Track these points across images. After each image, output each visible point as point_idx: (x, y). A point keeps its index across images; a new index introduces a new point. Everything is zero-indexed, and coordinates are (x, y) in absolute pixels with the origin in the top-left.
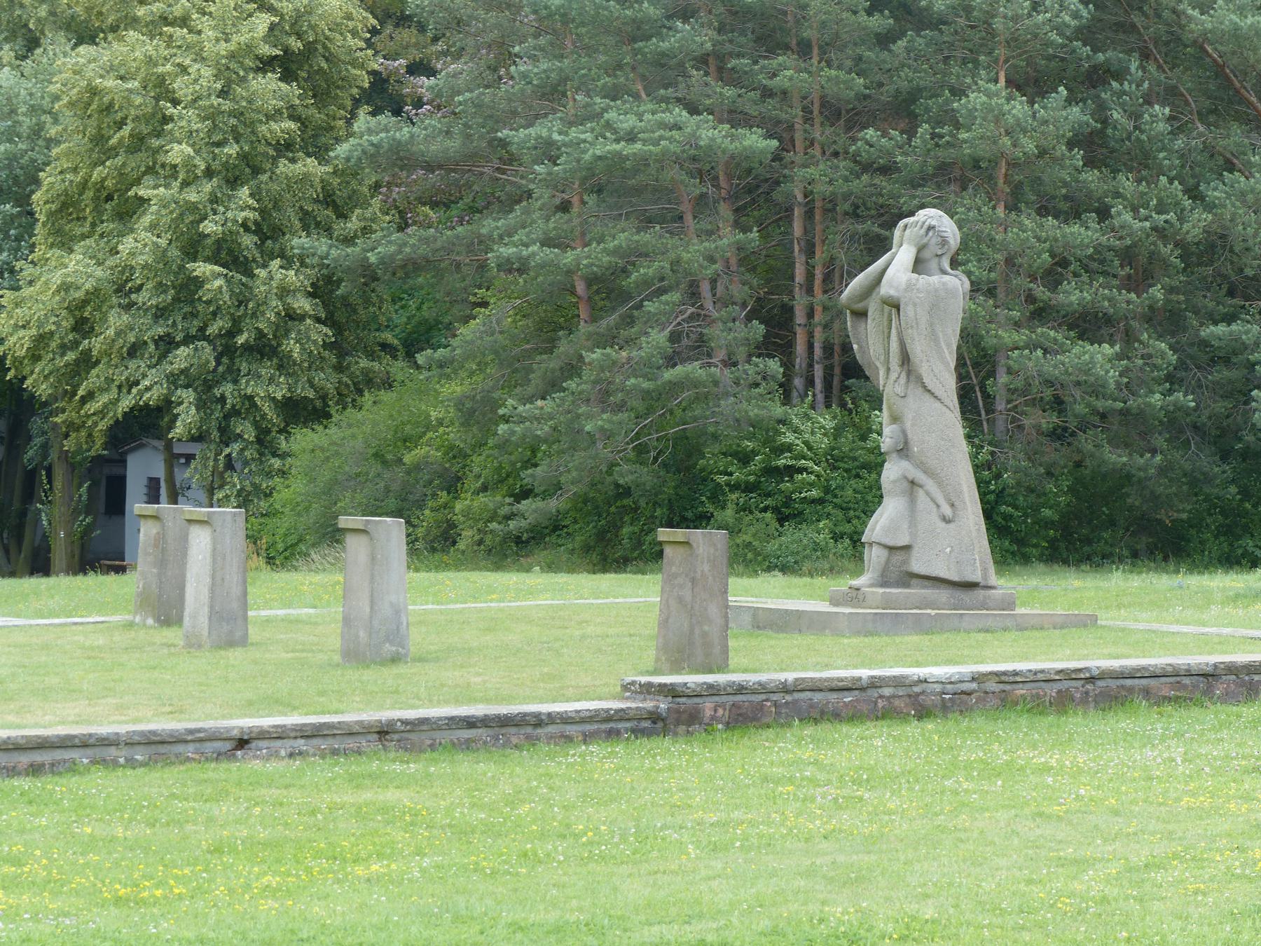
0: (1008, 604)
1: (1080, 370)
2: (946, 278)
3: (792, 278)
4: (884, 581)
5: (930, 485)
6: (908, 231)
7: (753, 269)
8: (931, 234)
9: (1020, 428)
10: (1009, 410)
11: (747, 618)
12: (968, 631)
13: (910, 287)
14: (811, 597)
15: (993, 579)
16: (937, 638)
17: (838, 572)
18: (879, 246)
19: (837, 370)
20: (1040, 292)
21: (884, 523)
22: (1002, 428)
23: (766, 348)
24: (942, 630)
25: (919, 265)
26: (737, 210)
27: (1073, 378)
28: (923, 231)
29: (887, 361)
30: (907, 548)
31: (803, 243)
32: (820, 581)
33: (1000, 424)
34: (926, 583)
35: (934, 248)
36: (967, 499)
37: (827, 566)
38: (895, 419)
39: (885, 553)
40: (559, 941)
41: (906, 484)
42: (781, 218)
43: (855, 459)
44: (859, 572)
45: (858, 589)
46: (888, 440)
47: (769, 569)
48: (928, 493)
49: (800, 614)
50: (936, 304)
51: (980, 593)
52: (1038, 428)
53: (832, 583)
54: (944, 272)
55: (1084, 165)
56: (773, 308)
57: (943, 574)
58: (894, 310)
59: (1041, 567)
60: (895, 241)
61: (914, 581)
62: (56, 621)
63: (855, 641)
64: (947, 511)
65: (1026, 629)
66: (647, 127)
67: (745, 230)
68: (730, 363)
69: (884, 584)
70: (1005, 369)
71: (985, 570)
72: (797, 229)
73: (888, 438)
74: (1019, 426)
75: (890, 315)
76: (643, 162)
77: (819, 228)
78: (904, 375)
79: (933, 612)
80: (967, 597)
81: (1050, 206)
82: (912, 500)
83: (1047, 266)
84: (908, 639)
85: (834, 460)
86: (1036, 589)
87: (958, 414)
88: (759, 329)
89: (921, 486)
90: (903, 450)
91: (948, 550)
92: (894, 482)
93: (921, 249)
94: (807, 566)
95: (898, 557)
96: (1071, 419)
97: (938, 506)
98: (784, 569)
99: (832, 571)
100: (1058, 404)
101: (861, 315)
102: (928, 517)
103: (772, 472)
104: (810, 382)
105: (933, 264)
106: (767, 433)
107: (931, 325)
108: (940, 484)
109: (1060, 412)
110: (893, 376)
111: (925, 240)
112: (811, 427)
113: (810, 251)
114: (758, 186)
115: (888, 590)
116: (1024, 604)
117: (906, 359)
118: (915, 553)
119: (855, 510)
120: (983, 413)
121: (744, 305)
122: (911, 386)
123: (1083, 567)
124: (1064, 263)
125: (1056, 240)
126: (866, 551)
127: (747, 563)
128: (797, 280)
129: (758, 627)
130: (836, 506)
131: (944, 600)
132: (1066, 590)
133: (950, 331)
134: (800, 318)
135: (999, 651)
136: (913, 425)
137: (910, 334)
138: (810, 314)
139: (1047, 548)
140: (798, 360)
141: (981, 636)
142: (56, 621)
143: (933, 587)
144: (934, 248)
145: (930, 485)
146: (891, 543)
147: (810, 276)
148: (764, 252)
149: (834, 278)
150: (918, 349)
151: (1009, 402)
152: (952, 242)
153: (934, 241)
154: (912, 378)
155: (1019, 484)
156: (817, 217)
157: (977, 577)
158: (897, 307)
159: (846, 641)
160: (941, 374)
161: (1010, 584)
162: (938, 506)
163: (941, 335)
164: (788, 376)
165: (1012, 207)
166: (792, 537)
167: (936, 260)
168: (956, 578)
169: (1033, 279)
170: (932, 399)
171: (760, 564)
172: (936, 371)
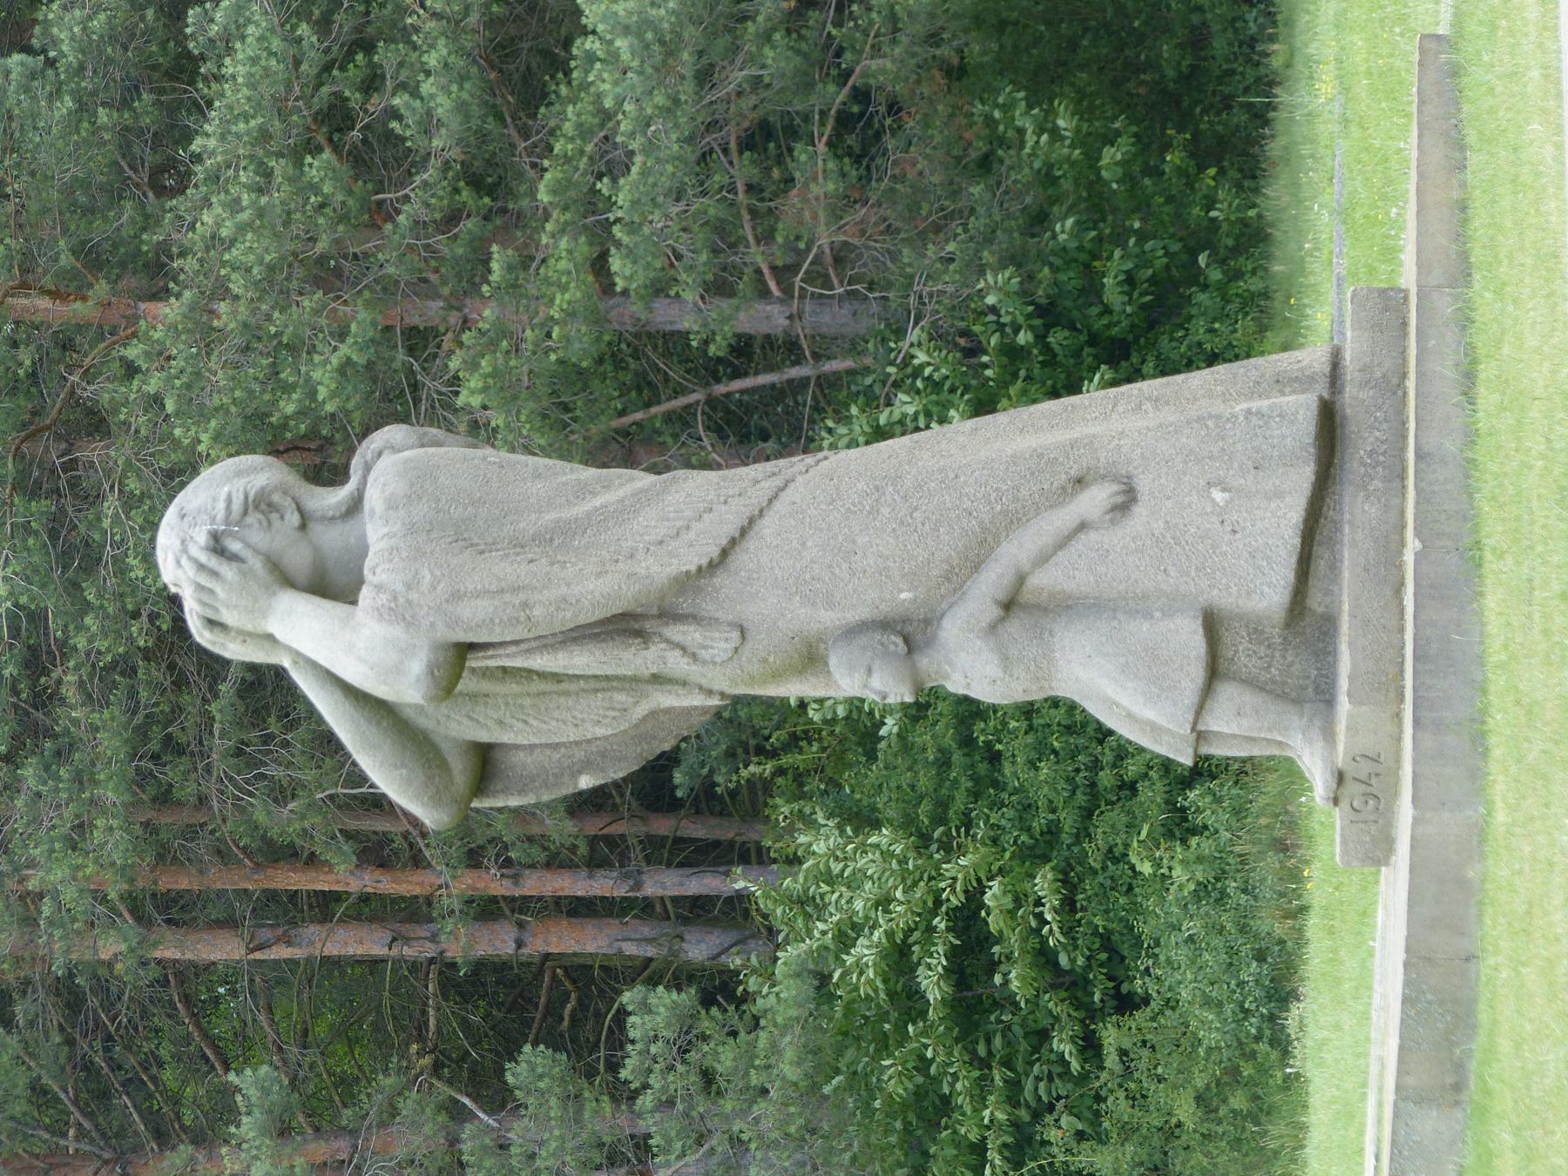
0: (1386, 309)
1: (663, 69)
2: (374, 498)
3: (375, 963)
4: (1317, 696)
5: (1015, 551)
6: (228, 617)
7: (347, 1086)
8: (234, 546)
9: (841, 256)
10: (787, 291)
11: (1429, 1123)
12: (1470, 437)
13: (399, 612)
14: (1366, 914)
15: (1312, 356)
16: (1493, 533)
17: (1292, 825)
18: (268, 691)
19: (662, 826)
20: (419, 199)
21: (1138, 698)
22: (845, 311)
23: (592, 1041)
24: (1468, 516)
25: (333, 584)
26: (162, 1137)
27: (687, 91)
28: (228, 571)
29: (632, 683)
30: (1212, 624)
31: (265, 934)
32: (1318, 887)
33: (833, 318)
34: (1320, 566)
35: (281, 536)
36: (1062, 436)
37: (1272, 860)
38: (811, 658)
39: (1228, 693)
41: (1014, 627)
42: (187, 999)
43: (944, 763)
44: (1292, 774)
45: (1341, 778)
46: (876, 682)
47: (1282, 1045)
48: (1043, 559)
49: (1417, 959)
50: (455, 530)
51: (1353, 397)
52: (841, 205)
53: (1321, 847)
54: (355, 506)
55: (28, 50)
56: (465, 1024)
57: (1293, 512)
58: (474, 662)
59: (1275, 193)
60: (258, 656)
61: (1316, 602)
62: (1412, 425)
63: (1500, 787)
64: (1096, 499)
65: (1464, 256)
67: (224, 1109)
69: (1324, 696)
70: (660, 304)
71: (1282, 382)
72: (223, 949)
73: (863, 680)
74: (838, 261)
75: (486, 673)
77: (221, 880)
78: (675, 632)
79: (1412, 545)
80: (1363, 439)
81: (150, 158)
82: (1063, 607)
83: (345, 170)
84: (1494, 625)
85: (932, 833)
86: (1343, 214)
87: (794, 465)
88: (533, 1068)
89: (1021, 579)
90: (909, 634)
91: (1218, 496)
92: (1006, 662)
93: (285, 579)
94: (1269, 924)
95: (1241, 652)
96: (815, 101)
97: (1082, 527)
98: (1281, 993)
99: (1287, 843)
100: (768, 138)
101: (486, 762)
102: (1108, 558)
104: (697, 910)
105: (331, 538)
106: (856, 1029)
107: (519, 545)
108: (1013, 521)
109: (792, 133)
110: (677, 664)
111: (256, 563)
112: (846, 886)
114: (88, 1066)
115: (1343, 684)
116: (1390, 253)
117: (626, 626)
118: (1226, 598)
119: (1096, 765)
120: (795, 372)
121: (457, 1114)
122: (708, 608)
123: (1276, 62)
124: (336, 118)
125: (264, 136)
126: (1218, 750)
127: (1260, 1111)
128: (378, 950)
129: (1458, 1087)
130: (1083, 834)
131: (1373, 510)
132: (1345, 122)
133: (538, 488)
134: (498, 942)
135: (1532, 342)
136: (830, 604)
137: (546, 613)
138: (486, 910)
139: (1222, 172)
140: (630, 949)
141: (1486, 397)
142: (1412, 425)
143: (1333, 543)
144: (281, 536)
146: (1195, 673)
147: (369, 909)
148: (293, 1051)
149: (383, 841)
150: (594, 587)
151: (764, 293)
152: (260, 480)
153: (257, 537)
154: (685, 606)
155: (1014, 259)
156: (183, 883)
157: (1302, 408)
158: (465, 649)
159: (1501, 817)
160: (668, 515)
161: (1329, 291)
162: (1082, 527)
164: (680, 977)
165: (156, 274)
166: (1184, 970)
167: (316, 529)
168: (1304, 476)
169: (381, 214)
170: (751, 543)
171: (1263, 1070)
172: (661, 531)
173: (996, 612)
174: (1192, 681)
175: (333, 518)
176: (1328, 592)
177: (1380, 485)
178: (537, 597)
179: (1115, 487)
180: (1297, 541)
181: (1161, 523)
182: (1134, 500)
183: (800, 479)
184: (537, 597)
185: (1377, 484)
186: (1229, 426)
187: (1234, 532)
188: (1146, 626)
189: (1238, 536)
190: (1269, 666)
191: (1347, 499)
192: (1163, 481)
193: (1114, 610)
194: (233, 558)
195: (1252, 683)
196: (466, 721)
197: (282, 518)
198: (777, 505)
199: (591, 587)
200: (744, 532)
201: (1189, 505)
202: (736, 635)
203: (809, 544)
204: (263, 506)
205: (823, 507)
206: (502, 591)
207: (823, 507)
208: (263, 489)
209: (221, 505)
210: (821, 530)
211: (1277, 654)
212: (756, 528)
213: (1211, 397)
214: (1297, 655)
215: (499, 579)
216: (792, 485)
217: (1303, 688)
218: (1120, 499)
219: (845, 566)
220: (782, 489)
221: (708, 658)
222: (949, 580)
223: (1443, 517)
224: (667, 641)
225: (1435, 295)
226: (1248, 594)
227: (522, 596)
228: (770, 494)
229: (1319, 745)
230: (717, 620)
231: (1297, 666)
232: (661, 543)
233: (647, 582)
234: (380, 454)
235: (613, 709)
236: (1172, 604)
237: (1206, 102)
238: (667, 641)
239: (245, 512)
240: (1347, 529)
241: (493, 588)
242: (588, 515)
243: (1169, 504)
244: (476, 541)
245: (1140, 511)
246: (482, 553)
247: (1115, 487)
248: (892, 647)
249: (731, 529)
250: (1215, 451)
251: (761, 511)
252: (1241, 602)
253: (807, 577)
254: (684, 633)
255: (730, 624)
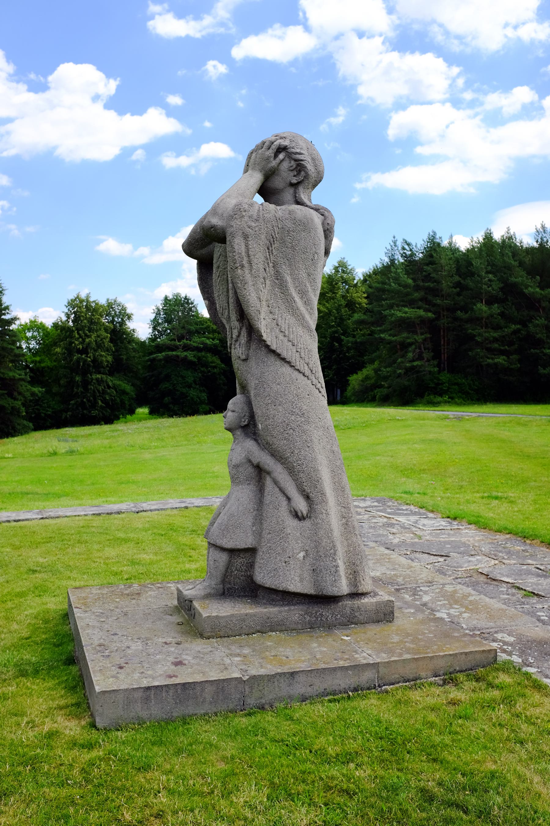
5: (279, 472)
8: (281, 156)
28: (270, 153)
30: (252, 551)
40: (66, 823)
41: (250, 470)
64: (302, 506)
66: (408, 312)
68: (428, 361)
72: (442, 334)
76: (408, 318)
78: (244, 333)
91: (302, 554)
95: (240, 561)
103: (438, 384)
108: (291, 471)
111: (274, 163)
113: (444, 338)
118: (260, 559)
122: (253, 346)
136: (255, 396)
145: (279, 472)
146: (230, 545)
153: (285, 165)
162: (289, 499)
163: (289, 279)
167: (291, 190)
168: (312, 592)
170: (279, 363)
172: (284, 326)
173: (255, 463)
174: (226, 543)
175: (296, 197)
176: (264, 598)
177: (307, 619)
178: (247, 272)
179: (305, 513)
180: (281, 589)
181: (289, 531)
182: (300, 520)
183: (309, 382)
184: (247, 272)
185: (308, 618)
186: (331, 559)
187: (286, 562)
188: (250, 523)
189: (284, 564)
190: (237, 570)
191: (301, 607)
192: (308, 531)
193: (258, 510)
194: (276, 156)
195: (228, 567)
196: (219, 253)
197: (294, 176)
198: (296, 373)
199: (252, 295)
200: (284, 359)
201: (298, 543)
202: (243, 357)
203: (278, 386)
204: (299, 168)
205: (295, 392)
206: (249, 256)
207: (295, 392)
208: (306, 167)
209: (298, 151)
210: (284, 391)
211: (243, 573)
212: (285, 364)
213: (348, 546)
214: (244, 581)
215: (254, 255)
216: (306, 378)
217: (230, 583)
218: (300, 514)
219: (270, 401)
220: (304, 375)
221: (236, 346)
222: (267, 443)
223: (261, 688)
224: (241, 329)
225: (374, 671)
226: (260, 567)
227: (246, 265)
228: (302, 369)
229: (203, 593)
230: (249, 349)
231: (239, 581)
232: (278, 325)
233: (256, 319)
234: (322, 215)
235: (223, 310)
236: (259, 534)
237: (473, 542)
238: (241, 329)
239: (296, 160)
240: (286, 608)
241: (250, 253)
242: (290, 295)
243: (298, 534)
244: (273, 246)
245: (295, 523)
246: (268, 249)
247: (305, 513)
248: (243, 420)
249: (284, 354)
250: (320, 553)
251: (293, 366)
252: (257, 563)
253: (265, 386)
254: (244, 336)
255: (248, 354)
